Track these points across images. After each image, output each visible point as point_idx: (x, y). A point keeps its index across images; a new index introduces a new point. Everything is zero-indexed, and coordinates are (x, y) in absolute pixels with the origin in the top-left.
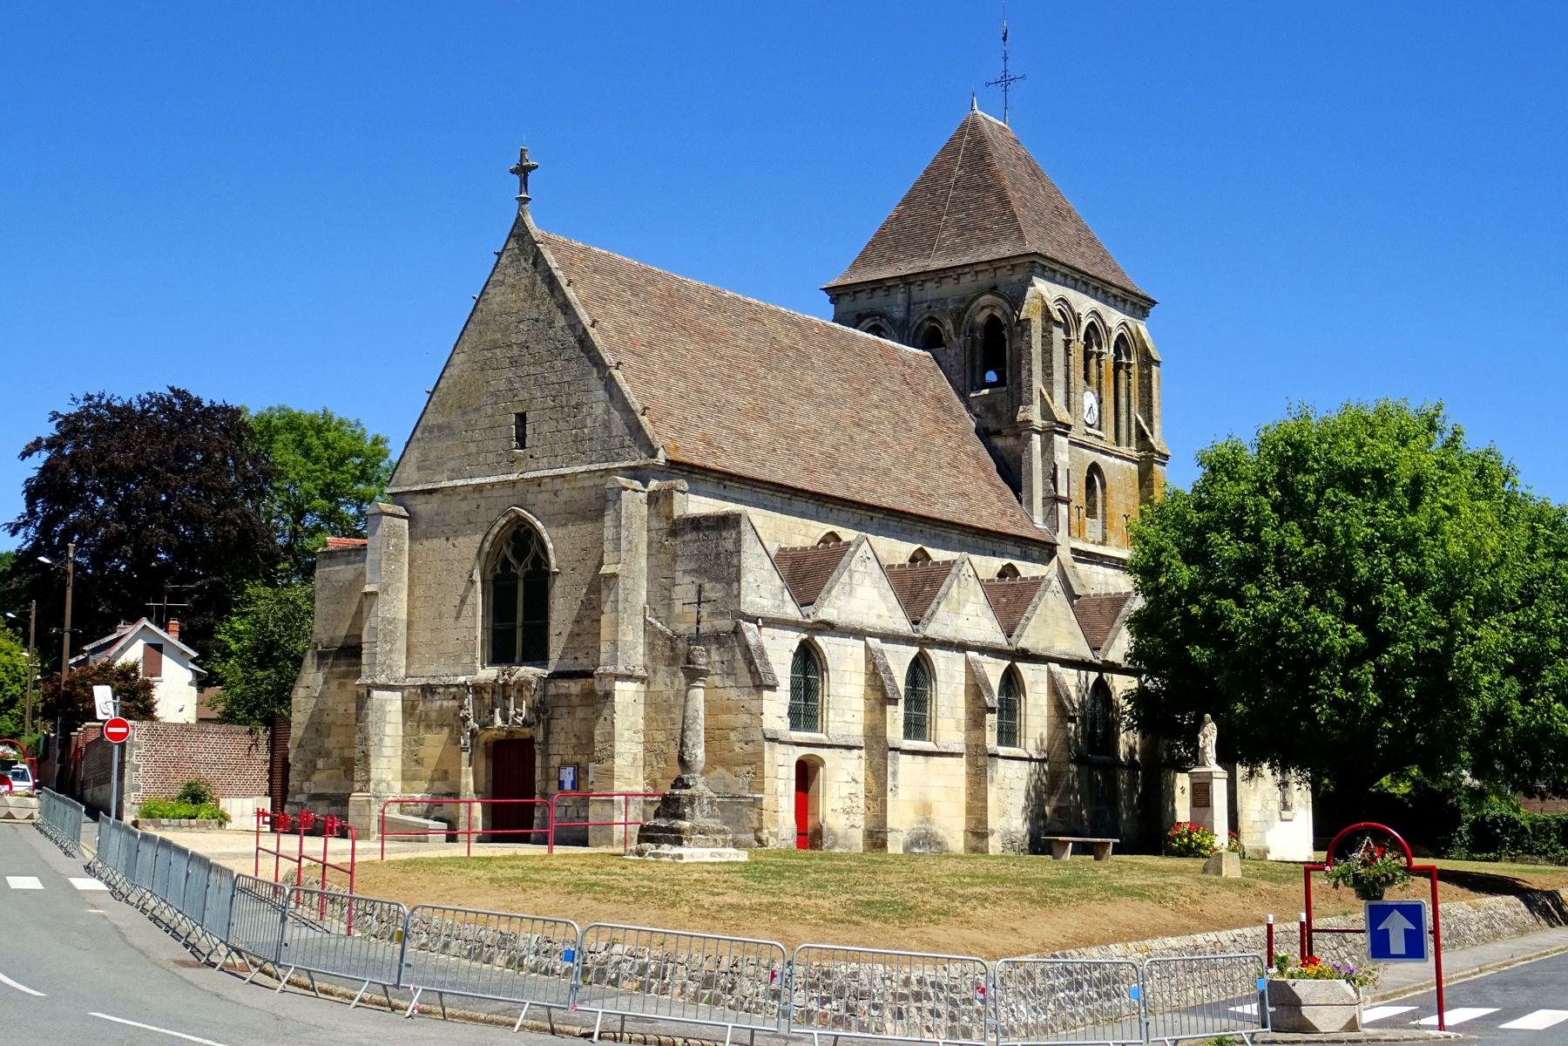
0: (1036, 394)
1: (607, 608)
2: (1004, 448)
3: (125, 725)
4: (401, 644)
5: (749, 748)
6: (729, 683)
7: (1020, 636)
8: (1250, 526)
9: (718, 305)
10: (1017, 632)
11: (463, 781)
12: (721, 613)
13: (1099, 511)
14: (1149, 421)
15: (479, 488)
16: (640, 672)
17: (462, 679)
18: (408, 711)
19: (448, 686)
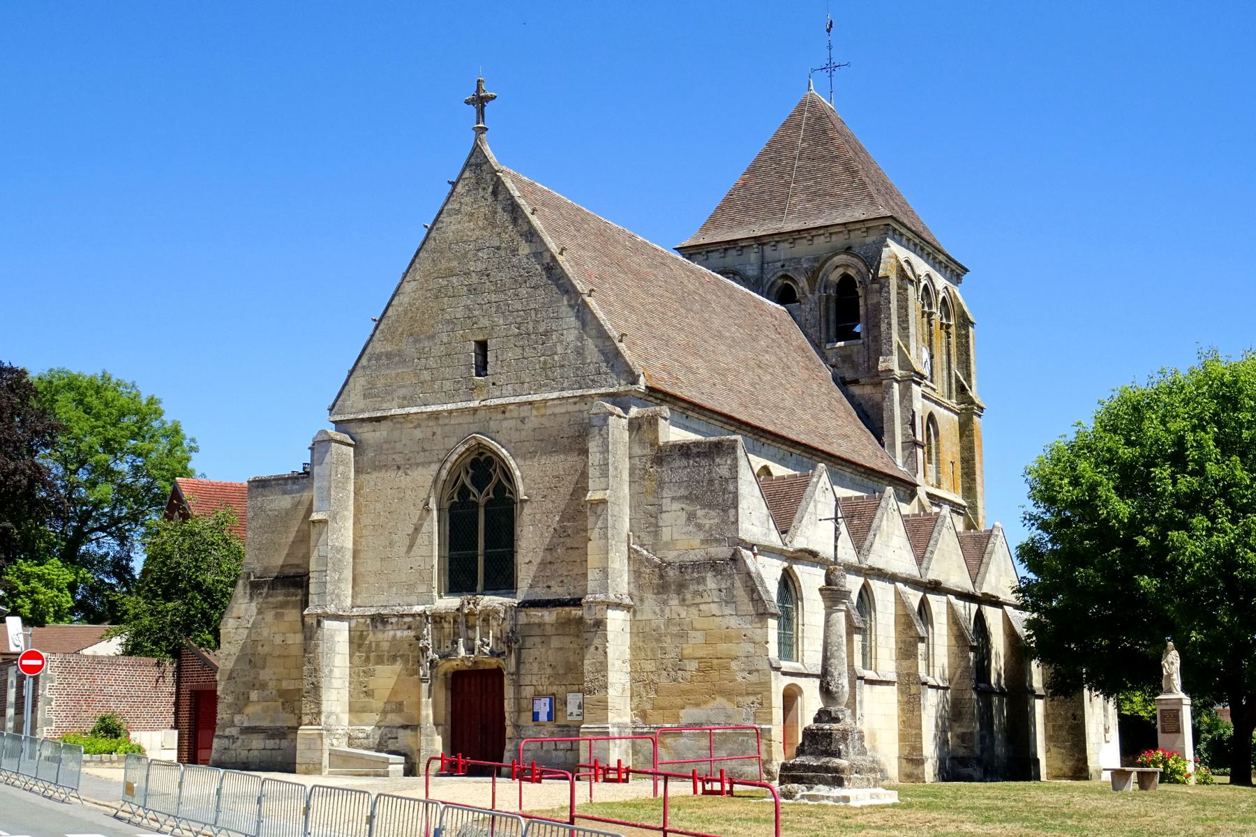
0: (895, 346)
1: (594, 534)
2: (862, 396)
3: (40, 657)
4: (348, 574)
5: (753, 678)
6: (728, 611)
8: (1193, 461)
9: (637, 248)
11: (424, 713)
12: (717, 540)
13: (934, 457)
14: (968, 377)
15: (435, 416)
16: (627, 601)
17: (418, 609)
18: (357, 642)
19: (402, 616)
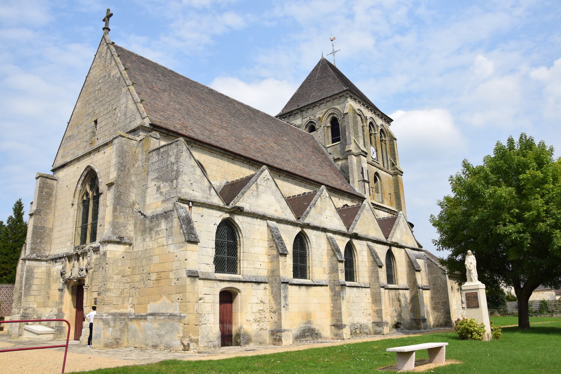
0: (353, 141)
7: (353, 228)
10: (352, 226)
13: (380, 191)
